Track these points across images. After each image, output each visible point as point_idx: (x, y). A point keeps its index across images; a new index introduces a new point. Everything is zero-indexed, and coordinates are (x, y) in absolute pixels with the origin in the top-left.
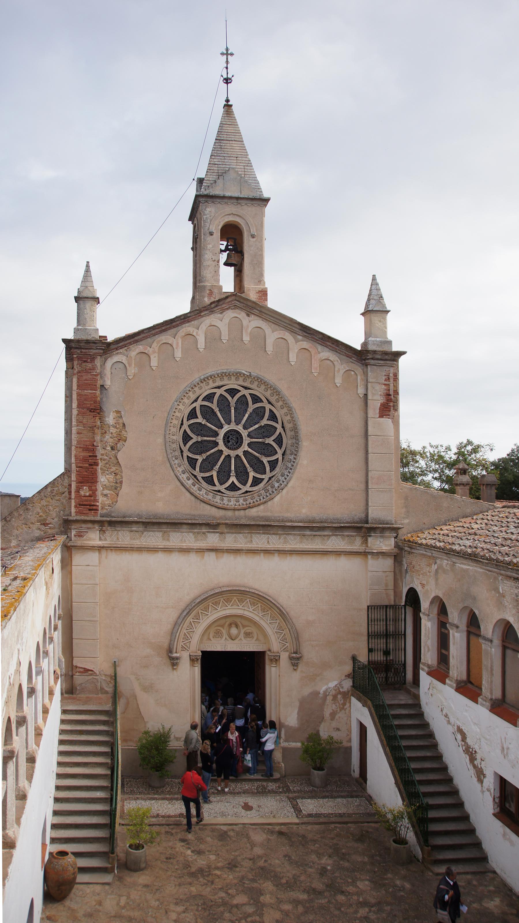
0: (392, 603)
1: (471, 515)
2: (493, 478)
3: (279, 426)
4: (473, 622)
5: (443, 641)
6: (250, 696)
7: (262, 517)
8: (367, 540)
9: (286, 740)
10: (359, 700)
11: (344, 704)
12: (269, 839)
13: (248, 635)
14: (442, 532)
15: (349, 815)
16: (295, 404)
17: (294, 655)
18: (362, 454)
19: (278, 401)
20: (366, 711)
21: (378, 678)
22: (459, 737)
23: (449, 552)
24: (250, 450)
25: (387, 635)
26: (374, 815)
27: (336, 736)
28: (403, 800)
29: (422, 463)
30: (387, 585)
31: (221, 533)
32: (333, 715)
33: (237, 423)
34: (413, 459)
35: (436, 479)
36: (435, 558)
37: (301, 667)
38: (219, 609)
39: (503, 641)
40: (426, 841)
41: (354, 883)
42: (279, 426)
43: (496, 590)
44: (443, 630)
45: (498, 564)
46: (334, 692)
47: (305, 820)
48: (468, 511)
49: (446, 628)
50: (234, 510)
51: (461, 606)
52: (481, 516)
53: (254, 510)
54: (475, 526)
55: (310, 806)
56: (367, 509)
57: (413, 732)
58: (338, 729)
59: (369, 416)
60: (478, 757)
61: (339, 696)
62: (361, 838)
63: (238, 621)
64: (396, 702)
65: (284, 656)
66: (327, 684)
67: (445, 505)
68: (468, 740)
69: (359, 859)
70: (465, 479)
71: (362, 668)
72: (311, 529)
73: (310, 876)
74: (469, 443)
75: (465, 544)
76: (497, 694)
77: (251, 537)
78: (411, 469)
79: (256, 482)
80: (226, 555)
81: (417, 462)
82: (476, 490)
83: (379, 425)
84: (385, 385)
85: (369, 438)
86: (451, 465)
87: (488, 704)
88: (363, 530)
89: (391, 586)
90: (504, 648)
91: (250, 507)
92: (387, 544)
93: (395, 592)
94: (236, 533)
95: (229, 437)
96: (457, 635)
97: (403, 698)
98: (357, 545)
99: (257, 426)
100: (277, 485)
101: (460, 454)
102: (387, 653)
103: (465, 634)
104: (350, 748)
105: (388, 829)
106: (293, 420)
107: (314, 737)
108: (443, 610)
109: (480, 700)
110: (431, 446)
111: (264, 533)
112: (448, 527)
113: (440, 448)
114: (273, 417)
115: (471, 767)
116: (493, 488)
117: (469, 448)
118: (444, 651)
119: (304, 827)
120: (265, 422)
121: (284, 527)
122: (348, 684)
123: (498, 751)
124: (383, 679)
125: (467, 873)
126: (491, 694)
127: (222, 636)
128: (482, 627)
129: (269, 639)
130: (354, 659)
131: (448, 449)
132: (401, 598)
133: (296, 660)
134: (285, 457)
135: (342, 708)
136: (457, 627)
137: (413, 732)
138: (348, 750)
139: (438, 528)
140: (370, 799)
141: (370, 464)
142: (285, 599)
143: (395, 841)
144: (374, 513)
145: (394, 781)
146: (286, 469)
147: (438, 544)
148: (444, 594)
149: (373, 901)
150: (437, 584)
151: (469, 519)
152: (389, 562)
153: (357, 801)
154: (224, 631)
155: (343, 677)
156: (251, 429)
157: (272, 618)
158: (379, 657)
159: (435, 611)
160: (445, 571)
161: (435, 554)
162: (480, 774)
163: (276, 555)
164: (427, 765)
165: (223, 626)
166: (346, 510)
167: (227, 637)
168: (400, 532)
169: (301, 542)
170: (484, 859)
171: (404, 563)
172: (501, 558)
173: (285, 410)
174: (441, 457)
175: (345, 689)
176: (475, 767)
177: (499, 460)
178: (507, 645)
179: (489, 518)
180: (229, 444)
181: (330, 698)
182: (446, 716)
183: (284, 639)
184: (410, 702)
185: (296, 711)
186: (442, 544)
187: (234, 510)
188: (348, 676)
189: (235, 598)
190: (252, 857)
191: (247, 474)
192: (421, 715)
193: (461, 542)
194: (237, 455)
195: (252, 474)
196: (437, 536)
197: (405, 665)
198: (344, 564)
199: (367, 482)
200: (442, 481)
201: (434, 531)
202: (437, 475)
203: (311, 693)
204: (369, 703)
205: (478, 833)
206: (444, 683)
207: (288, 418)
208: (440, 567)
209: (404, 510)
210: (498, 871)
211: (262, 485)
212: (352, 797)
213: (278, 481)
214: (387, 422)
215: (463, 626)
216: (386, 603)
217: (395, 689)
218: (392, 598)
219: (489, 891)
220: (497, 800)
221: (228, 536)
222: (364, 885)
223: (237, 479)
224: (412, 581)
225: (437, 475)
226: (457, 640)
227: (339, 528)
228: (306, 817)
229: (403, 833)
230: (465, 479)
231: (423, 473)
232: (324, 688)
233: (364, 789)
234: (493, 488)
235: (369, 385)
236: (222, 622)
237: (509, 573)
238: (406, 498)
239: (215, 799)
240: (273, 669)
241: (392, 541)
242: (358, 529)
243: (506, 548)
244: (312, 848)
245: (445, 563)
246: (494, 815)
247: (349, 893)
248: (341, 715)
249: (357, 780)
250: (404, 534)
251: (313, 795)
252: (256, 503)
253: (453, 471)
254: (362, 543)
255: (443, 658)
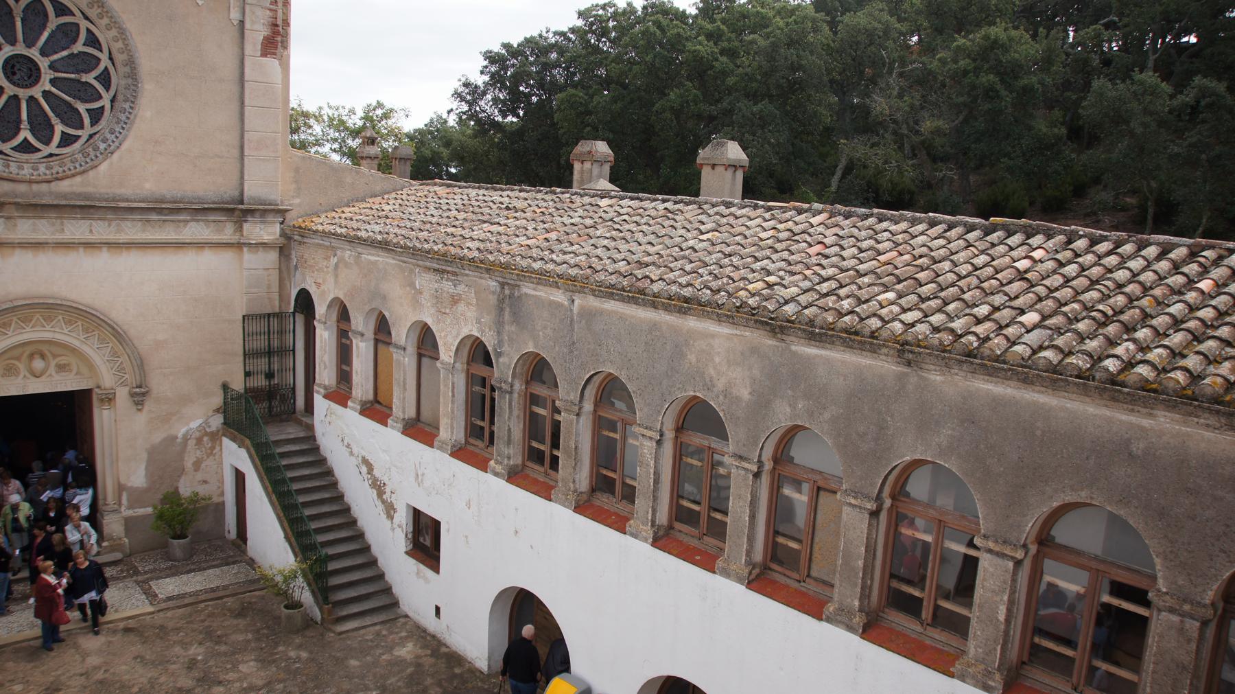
0: (277, 310)
1: (381, 194)
2: (409, 150)
3: (104, 57)
4: (382, 328)
5: (344, 354)
6: (70, 455)
7: (80, 194)
8: (241, 227)
9: (129, 508)
10: (234, 439)
11: (213, 448)
12: (110, 642)
13: (61, 368)
14: (344, 216)
15: (225, 588)
16: (131, 26)
17: (138, 390)
18: (235, 106)
19: (101, 16)
20: (243, 453)
21: (259, 409)
22: (364, 469)
23: (354, 241)
24: (54, 90)
25: (270, 353)
26: (258, 580)
27: (202, 490)
28: (296, 556)
29: (317, 129)
30: (269, 287)
31: (8, 218)
32: (197, 465)
33: (30, 44)
34: (305, 124)
35: (335, 151)
36: (334, 249)
37: (149, 405)
38: (10, 334)
39: (419, 348)
40: (326, 600)
41: (234, 667)
42: (104, 57)
43: (412, 285)
44: (344, 341)
45: (415, 253)
46: (198, 434)
47: (163, 605)
48: (378, 188)
49: (348, 338)
50: (30, 182)
51: (367, 308)
52: (393, 195)
53: (66, 183)
54: (386, 208)
55: (168, 587)
56: (242, 184)
57: (307, 472)
58: (205, 482)
59: (247, 52)
60: (388, 489)
61: (205, 439)
62: (241, 613)
63: (45, 348)
64: (283, 437)
65: (122, 394)
66: (188, 424)
67: (349, 180)
68: (376, 472)
69: (241, 637)
70: (373, 150)
71: (237, 399)
72: (160, 211)
73: (173, 674)
74: (380, 105)
75: (374, 230)
76: (411, 413)
77: (62, 224)
78: (303, 136)
79: (67, 140)
80: (18, 252)
81: (310, 127)
82: (385, 164)
83: (259, 67)
84: (271, 10)
85: (246, 85)
86: (355, 133)
87: (400, 426)
88: (237, 213)
89: (275, 288)
90: (420, 356)
91: (57, 179)
92: (269, 232)
93: (280, 296)
94: (34, 217)
95: (13, 67)
96: (362, 345)
97: (292, 431)
98: (228, 233)
99: (65, 53)
100: (102, 146)
101: (367, 118)
102: (270, 375)
103: (372, 343)
104: (223, 503)
105: (278, 594)
106: (127, 49)
107: (172, 498)
108: (344, 315)
109: (389, 421)
110: (330, 107)
111: (83, 218)
112: (352, 209)
113: (341, 110)
114: (93, 41)
115: (379, 503)
116: (408, 163)
117: (379, 112)
118: (344, 367)
119: (161, 615)
120: (79, 47)
121: (116, 209)
122: (217, 421)
123: (412, 479)
124: (266, 409)
125: (375, 624)
126: (404, 412)
127: (19, 373)
128: (393, 333)
129: (96, 369)
130: (225, 387)
131: (352, 112)
132: (289, 303)
133: (140, 396)
134: (116, 104)
135: (211, 453)
136: (362, 335)
137: (307, 472)
138: (220, 507)
139: (339, 210)
140: (252, 563)
141: (246, 121)
142: (120, 313)
143: (286, 607)
144: (253, 190)
145: (282, 535)
146: (118, 123)
147: (339, 230)
148: (345, 295)
149: (260, 683)
150: (336, 282)
151: (378, 199)
152: (273, 256)
153: (234, 569)
154: (21, 366)
155: (210, 413)
156: (56, 57)
157: (101, 340)
158: (259, 382)
159: (334, 317)
160: (347, 265)
161: (335, 243)
162: (390, 510)
163: (105, 249)
164: (326, 509)
165: (18, 359)
166: (210, 183)
167: (28, 375)
168: (288, 216)
169: (144, 231)
170: (395, 604)
171: (293, 256)
172: (419, 246)
173: (114, 32)
174: (342, 122)
175: (214, 429)
176: (383, 502)
177: (416, 131)
178: (423, 352)
179: (404, 197)
180: (18, 76)
181: (192, 443)
182: (348, 446)
183: (121, 369)
184: (302, 434)
185: (143, 467)
186: (344, 230)
187: (30, 182)
188: (218, 411)
189: (38, 315)
190: (83, 671)
191: (51, 128)
192: (316, 449)
193: (368, 227)
194: (44, 92)
195: (59, 128)
196: (337, 220)
197: (294, 389)
198: (209, 259)
199: (242, 147)
200: (344, 154)
201: (334, 214)
202: (336, 146)
203: (165, 440)
204: (248, 442)
205: (387, 578)
206: (345, 406)
207: (120, 45)
208: (341, 260)
209: (294, 186)
210: (410, 614)
211: (77, 146)
212: (227, 564)
213: (105, 140)
214: (272, 63)
215: (370, 334)
216: (269, 311)
217: (282, 421)
218: (277, 303)
219: (401, 638)
220: (410, 536)
221: (20, 222)
222: (249, 667)
223: (34, 134)
224: (304, 280)
225: (336, 146)
226: (362, 350)
227: (201, 210)
228: (165, 601)
229: (296, 596)
230: (373, 150)
231: (318, 143)
232: (183, 430)
233: (244, 552)
234: (408, 163)
235: (248, 8)
236: (16, 352)
237: (428, 264)
238: (297, 170)
239: (17, 608)
240: (106, 413)
241: (277, 228)
242: (229, 211)
243: (425, 233)
244: (175, 638)
245: (348, 254)
246: (407, 553)
247: (229, 681)
248: (209, 462)
249: (233, 542)
250: (294, 219)
251: (173, 572)
252: (69, 173)
253: (358, 141)
254: (235, 231)
255: (344, 377)
